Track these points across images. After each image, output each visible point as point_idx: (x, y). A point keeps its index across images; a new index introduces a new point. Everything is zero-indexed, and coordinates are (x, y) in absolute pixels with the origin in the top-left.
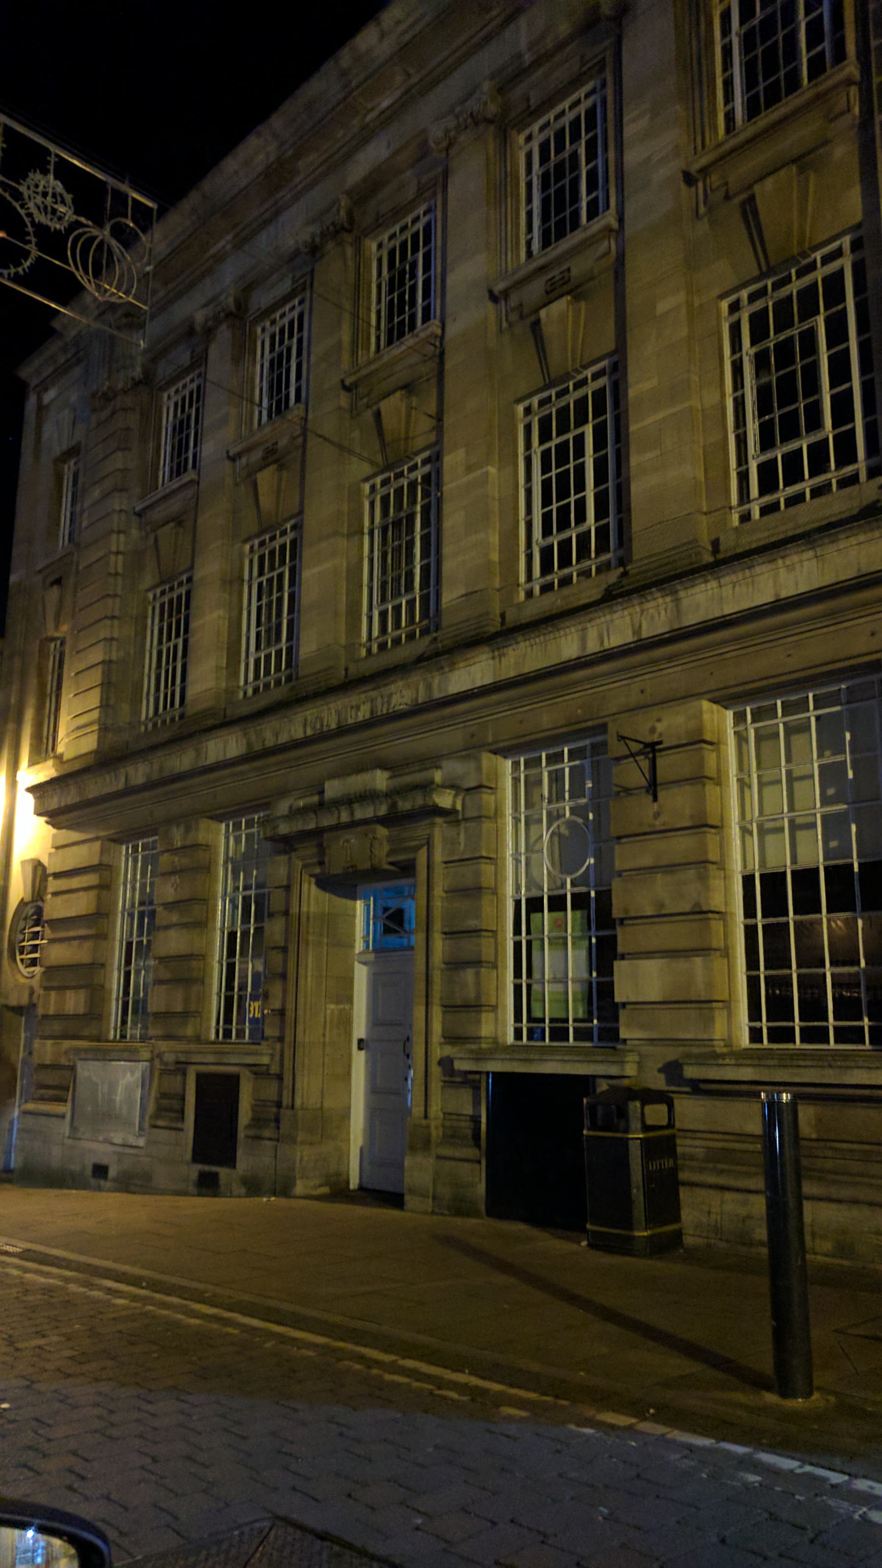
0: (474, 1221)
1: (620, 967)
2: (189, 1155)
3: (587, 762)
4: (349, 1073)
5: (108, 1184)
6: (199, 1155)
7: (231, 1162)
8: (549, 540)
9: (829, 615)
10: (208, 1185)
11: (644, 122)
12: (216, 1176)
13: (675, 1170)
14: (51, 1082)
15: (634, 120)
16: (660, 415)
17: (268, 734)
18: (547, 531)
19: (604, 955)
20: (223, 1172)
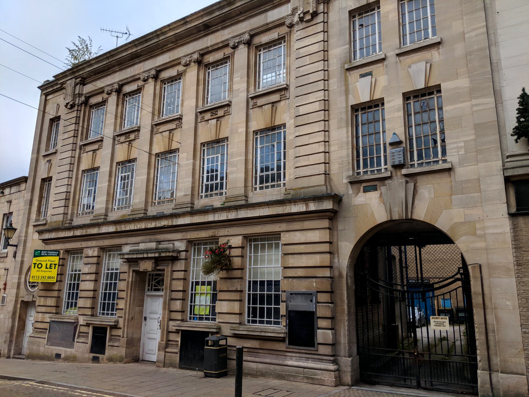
0: (175, 370)
1: (218, 303)
2: (89, 351)
3: (253, 243)
4: (141, 327)
5: (61, 360)
6: (92, 351)
7: (103, 353)
8: (208, 183)
9: (230, 89)
10: (96, 360)
11: (238, 79)
12: (98, 358)
13: (226, 356)
14: (298, 234)
15: (237, 77)
16: (238, 159)
17: (216, 233)
18: (207, 181)
19: (214, 298)
20: (100, 356)
